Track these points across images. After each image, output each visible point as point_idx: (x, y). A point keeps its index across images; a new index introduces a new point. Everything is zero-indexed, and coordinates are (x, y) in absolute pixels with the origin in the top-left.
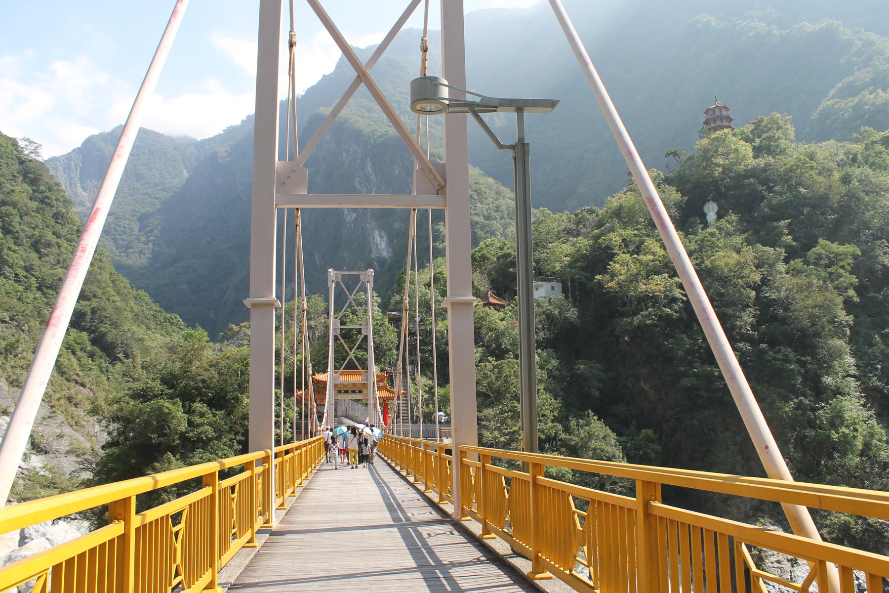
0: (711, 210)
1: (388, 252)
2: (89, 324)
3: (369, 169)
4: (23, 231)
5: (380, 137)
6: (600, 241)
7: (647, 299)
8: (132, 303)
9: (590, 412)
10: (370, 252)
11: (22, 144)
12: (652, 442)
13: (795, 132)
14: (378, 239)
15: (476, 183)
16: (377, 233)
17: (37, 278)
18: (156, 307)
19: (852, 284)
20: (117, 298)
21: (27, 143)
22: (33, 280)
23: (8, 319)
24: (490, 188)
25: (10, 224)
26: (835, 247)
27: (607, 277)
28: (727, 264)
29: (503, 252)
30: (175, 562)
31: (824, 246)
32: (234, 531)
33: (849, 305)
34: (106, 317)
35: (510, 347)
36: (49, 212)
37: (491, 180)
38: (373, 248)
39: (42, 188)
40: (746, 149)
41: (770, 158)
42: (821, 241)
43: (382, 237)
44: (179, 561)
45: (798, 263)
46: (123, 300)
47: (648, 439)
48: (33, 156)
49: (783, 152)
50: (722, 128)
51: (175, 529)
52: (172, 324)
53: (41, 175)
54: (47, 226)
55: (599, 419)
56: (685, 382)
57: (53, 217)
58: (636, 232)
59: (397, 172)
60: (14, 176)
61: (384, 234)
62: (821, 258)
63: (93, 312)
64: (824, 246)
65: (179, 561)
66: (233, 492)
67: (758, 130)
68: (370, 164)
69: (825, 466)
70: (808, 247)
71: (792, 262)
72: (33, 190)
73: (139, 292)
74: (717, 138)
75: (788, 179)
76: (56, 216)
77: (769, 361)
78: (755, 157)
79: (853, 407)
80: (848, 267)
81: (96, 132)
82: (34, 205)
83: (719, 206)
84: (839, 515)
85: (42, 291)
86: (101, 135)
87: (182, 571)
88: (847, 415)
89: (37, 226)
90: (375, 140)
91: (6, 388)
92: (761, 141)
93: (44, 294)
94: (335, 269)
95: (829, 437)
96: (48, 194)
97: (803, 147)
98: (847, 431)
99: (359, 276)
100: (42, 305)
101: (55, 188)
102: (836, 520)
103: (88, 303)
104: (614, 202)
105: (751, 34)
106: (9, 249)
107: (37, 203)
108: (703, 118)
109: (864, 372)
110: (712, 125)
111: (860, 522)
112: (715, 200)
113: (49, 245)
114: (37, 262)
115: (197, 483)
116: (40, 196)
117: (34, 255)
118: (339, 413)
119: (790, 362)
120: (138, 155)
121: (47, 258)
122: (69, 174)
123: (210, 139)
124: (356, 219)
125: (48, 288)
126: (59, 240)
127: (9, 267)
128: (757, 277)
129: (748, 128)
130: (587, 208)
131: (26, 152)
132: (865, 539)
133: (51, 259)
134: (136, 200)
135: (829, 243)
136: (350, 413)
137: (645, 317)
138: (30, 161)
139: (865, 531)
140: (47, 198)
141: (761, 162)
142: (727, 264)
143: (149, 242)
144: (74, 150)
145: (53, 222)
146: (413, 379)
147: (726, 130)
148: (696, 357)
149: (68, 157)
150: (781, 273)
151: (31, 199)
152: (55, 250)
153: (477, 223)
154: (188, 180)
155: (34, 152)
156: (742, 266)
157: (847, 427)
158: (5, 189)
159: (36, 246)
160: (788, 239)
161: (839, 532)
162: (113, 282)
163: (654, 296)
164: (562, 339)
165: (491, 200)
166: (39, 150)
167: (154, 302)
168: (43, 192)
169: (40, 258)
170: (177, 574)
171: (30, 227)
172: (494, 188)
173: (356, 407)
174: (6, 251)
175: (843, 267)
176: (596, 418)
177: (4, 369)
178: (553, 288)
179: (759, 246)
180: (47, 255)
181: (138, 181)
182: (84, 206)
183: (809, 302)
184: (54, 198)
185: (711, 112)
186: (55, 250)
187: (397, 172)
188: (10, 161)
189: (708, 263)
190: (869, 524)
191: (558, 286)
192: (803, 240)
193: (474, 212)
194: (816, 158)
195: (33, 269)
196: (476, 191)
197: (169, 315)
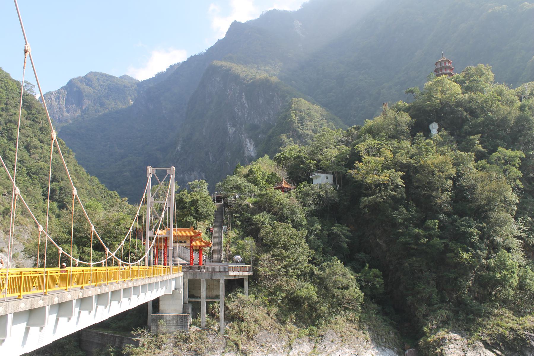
0: (434, 128)
1: (255, 153)
2: (58, 197)
3: (244, 100)
5: (251, 79)
6: (355, 148)
7: (379, 185)
8: (86, 184)
9: (336, 257)
10: (244, 153)
12: (378, 277)
13: (494, 76)
14: (248, 144)
15: (308, 109)
16: (248, 140)
17: (26, 167)
18: (102, 186)
19: (518, 176)
22: (24, 169)
23: (6, 193)
24: (317, 112)
25: (12, 134)
26: (509, 153)
28: (433, 164)
29: (300, 154)
31: (503, 152)
33: (515, 189)
34: (69, 193)
35: (288, 215)
36: (37, 127)
37: (318, 107)
38: (246, 150)
39: (34, 112)
40: (457, 88)
41: (472, 94)
42: (500, 148)
43: (251, 143)
45: (483, 162)
46: (81, 182)
47: (376, 276)
49: (482, 90)
50: (441, 74)
52: (112, 197)
53: (33, 104)
54: (35, 136)
55: (341, 262)
56: (402, 239)
57: (40, 130)
58: (379, 142)
59: (261, 102)
61: (252, 141)
62: (499, 160)
63: (61, 189)
64: (503, 152)
67: (469, 76)
68: (244, 97)
69: (495, 295)
70: (491, 152)
71: (479, 162)
72: (29, 114)
73: (93, 177)
74: (438, 81)
75: (483, 108)
76: (41, 129)
77: (457, 227)
78: (463, 93)
79: (515, 258)
80: (518, 166)
81: (76, 76)
82: (28, 122)
83: (439, 125)
84: (498, 328)
85: (30, 176)
86: (79, 78)
88: (508, 263)
89: (29, 136)
91: (3, 236)
92: (469, 83)
93: (31, 178)
94: (153, 166)
95: (495, 276)
96: (37, 116)
97: (497, 87)
98: (506, 273)
99: (166, 170)
100: (29, 184)
101: (42, 111)
102: (496, 332)
103: (58, 183)
104: (369, 123)
105: (490, 11)
106: (10, 149)
107: (30, 121)
108: (434, 67)
109: (528, 234)
110: (440, 73)
111: (512, 333)
112: (437, 122)
114: (27, 158)
116: (32, 116)
117: (26, 154)
118: (175, 255)
119: (471, 227)
120: (101, 91)
121: (34, 155)
122: (59, 102)
123: (147, 81)
124: (235, 131)
125: (33, 174)
126: (42, 144)
127: (10, 161)
128: (453, 172)
129: (461, 76)
130: (355, 126)
132: (515, 345)
133: (37, 156)
135: (505, 149)
136: (182, 255)
137: (379, 197)
138: (27, 95)
139: (515, 339)
140: (36, 118)
141: (466, 97)
142: (433, 164)
144: (62, 87)
145: (39, 133)
146: (226, 235)
147: (444, 76)
148: (411, 223)
149: (58, 92)
150: (471, 169)
151: (27, 119)
152: (39, 150)
153: (308, 135)
154: (133, 106)
156: (443, 163)
157: (507, 270)
158: (11, 113)
159: (27, 148)
160: (479, 147)
161: (497, 339)
162: (75, 171)
163: (385, 184)
164: (325, 211)
165: (317, 120)
166: (33, 88)
167: (102, 183)
168: (33, 114)
169: (30, 156)
171: (25, 136)
172: (320, 112)
173: (186, 252)
174: (8, 151)
175: (514, 165)
176: (339, 261)
177: (2, 224)
178: (327, 178)
179: (458, 152)
180: (34, 154)
181: (101, 107)
182: (68, 122)
183: (487, 188)
184: (41, 118)
185: (439, 64)
186: (39, 150)
187: (261, 102)
188: (14, 95)
189: (422, 162)
190: (518, 335)
191: (330, 177)
192: (490, 147)
193: (306, 128)
194: (499, 95)
195: (24, 162)
196: (307, 114)
197: (110, 192)
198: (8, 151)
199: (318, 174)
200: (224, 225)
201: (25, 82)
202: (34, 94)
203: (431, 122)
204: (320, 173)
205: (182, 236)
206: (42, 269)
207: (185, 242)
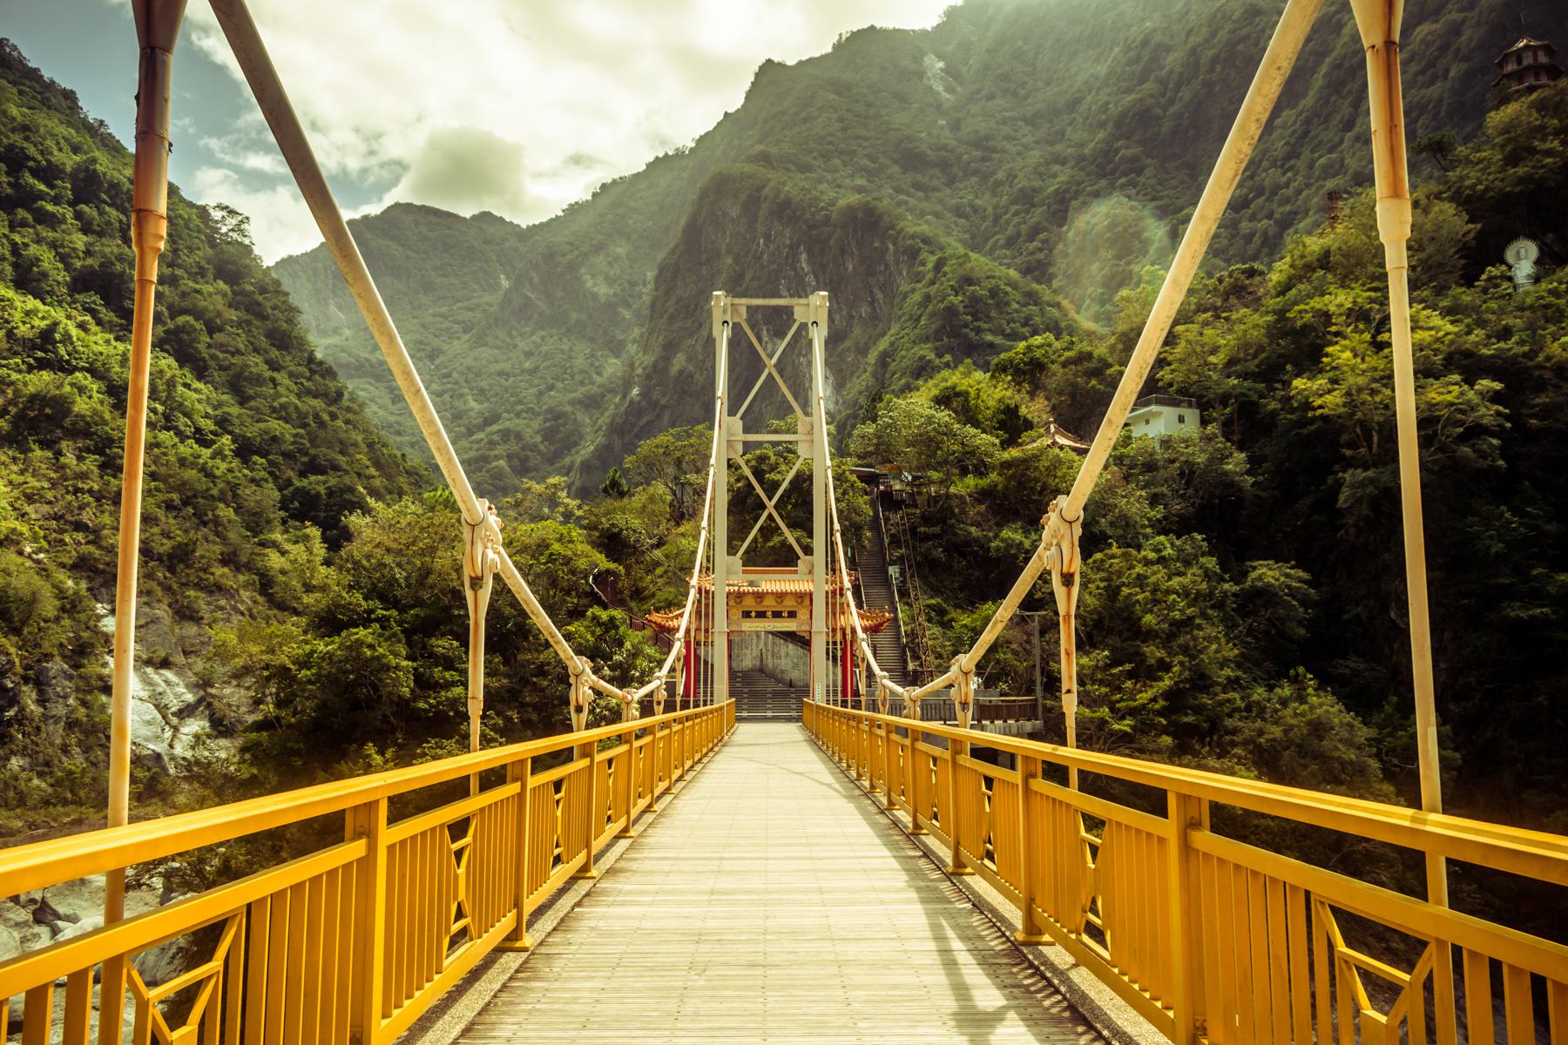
4: (213, 357)
11: (217, 215)
20: (372, 471)
21: (224, 213)
22: (226, 440)
27: (1321, 382)
30: (456, 897)
32: (556, 852)
44: (462, 896)
48: (235, 235)
51: (557, 797)
59: (850, 268)
60: (201, 268)
65: (462, 896)
66: (558, 790)
68: (804, 256)
72: (234, 292)
82: (233, 315)
83: (1541, 250)
87: (467, 908)
90: (813, 215)
94: (735, 288)
113: (258, 380)
115: (325, 830)
126: (276, 375)
131: (224, 230)
134: (423, 326)
143: (445, 392)
155: (238, 228)
170: (460, 915)
173: (783, 651)
174: (180, 388)
178: (1181, 419)
186: (268, 390)
187: (850, 268)
198: (180, 388)
199: (1154, 408)
200: (893, 563)
201: (220, 207)
202: (247, 241)
203: (1512, 237)
204: (1159, 402)
205: (780, 596)
206: (697, 710)
207: (792, 615)
